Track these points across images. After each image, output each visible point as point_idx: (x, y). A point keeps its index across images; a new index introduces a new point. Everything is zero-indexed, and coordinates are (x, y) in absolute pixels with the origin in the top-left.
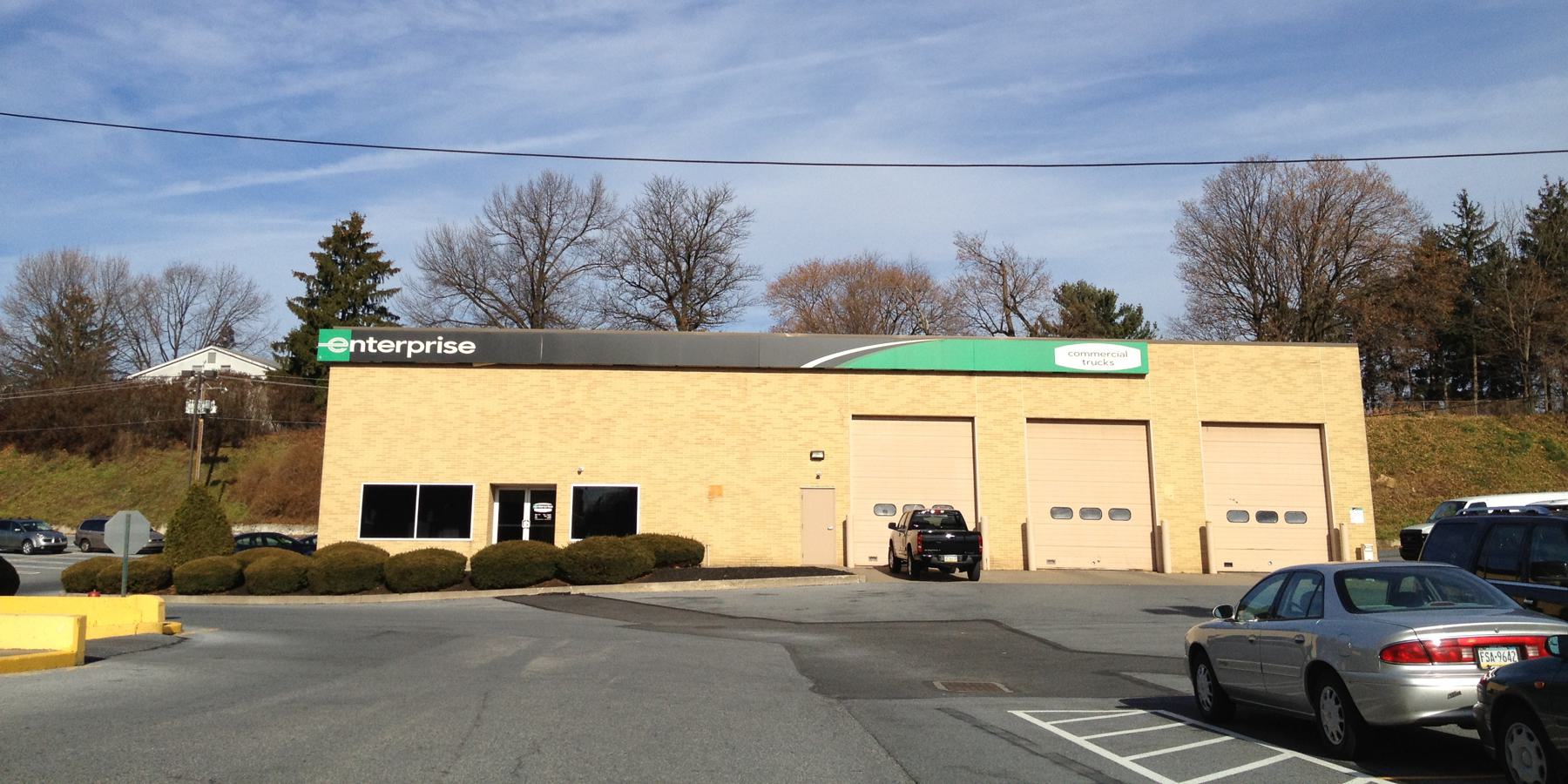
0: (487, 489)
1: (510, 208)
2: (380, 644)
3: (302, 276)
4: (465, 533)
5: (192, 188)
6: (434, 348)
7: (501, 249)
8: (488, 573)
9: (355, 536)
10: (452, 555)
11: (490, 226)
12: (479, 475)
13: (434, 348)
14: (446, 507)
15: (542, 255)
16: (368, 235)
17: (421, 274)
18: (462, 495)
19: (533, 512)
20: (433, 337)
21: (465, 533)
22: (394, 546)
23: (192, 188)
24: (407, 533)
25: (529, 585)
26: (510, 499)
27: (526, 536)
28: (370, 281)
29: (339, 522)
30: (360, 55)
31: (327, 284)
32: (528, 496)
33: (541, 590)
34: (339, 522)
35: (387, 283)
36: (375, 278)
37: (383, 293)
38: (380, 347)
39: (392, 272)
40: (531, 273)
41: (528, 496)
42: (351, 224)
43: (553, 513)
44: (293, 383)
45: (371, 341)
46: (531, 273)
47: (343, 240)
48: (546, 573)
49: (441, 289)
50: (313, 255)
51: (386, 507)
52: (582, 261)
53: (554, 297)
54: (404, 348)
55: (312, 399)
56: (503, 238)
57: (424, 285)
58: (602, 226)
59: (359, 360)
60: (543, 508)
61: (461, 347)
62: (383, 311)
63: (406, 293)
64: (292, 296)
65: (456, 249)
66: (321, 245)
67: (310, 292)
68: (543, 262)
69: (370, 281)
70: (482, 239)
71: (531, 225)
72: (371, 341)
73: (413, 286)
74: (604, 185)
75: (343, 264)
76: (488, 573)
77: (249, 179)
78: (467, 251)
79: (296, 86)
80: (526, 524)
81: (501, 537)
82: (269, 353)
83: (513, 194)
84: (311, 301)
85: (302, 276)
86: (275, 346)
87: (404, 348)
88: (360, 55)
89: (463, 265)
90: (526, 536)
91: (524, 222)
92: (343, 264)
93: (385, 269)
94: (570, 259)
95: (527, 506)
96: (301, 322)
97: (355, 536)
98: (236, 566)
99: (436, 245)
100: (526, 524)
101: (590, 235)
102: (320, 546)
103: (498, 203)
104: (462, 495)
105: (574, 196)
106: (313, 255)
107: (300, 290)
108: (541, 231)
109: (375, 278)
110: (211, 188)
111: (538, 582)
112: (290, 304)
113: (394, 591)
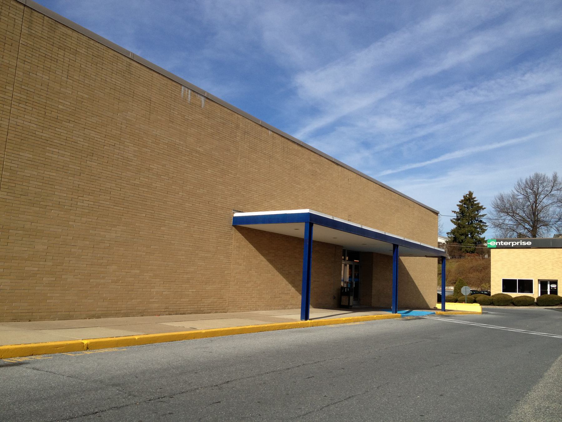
0: (537, 281)
1: (523, 187)
2: (526, 315)
3: (455, 212)
4: (531, 292)
5: (389, 172)
6: (519, 244)
7: (521, 201)
8: (540, 302)
9: (501, 292)
10: (530, 297)
11: (517, 193)
12: (535, 277)
13: (519, 244)
14: (526, 285)
15: (535, 202)
16: (475, 198)
17: (494, 209)
18: (530, 282)
19: (550, 287)
20: (519, 241)
21: (531, 292)
22: (513, 295)
23: (389, 172)
24: (515, 291)
25: (554, 306)
26: (543, 284)
27: (549, 293)
28: (476, 213)
29: (496, 288)
30: (443, 118)
31: (463, 214)
32: (549, 283)
33: (557, 307)
34: (496, 288)
35: (482, 213)
36: (478, 211)
37: (481, 216)
38: (504, 243)
39: (483, 209)
40: (532, 207)
41: (549, 283)
42: (469, 195)
43: (557, 287)
44: (455, 245)
45: (502, 242)
46: (532, 207)
47: (467, 200)
48: (558, 303)
49: (502, 214)
50: (458, 205)
51: (509, 285)
52: (550, 202)
53: (541, 215)
54: (511, 244)
55: (461, 250)
56: (521, 196)
57: (495, 213)
58: (558, 190)
59: (498, 247)
60: (554, 286)
61: (527, 243)
62: (481, 221)
63: (489, 215)
64: (452, 218)
65: (505, 201)
66: (460, 202)
67: (457, 217)
68: (536, 204)
69: (476, 213)
70: (514, 197)
71: (531, 191)
72: (502, 242)
73: (491, 213)
74: (558, 175)
75: (467, 208)
76: (540, 302)
77: (408, 167)
78: (509, 200)
79: (422, 133)
80: (549, 290)
81: (541, 294)
82: (446, 236)
83: (524, 181)
84: (458, 219)
85: (455, 212)
86: (448, 233)
87: (511, 244)
88: (443, 118)
89: (507, 205)
90: (549, 293)
91: (529, 191)
92: (467, 208)
93: (481, 208)
94: (546, 201)
95: (549, 285)
96: (455, 226)
97: (501, 292)
98: (473, 298)
99: (498, 200)
100: (549, 290)
101: (552, 193)
102: (492, 295)
103: (519, 185)
104: (530, 282)
105: (546, 180)
106: (458, 205)
107: (454, 216)
108: (534, 192)
109: (478, 211)
110: (394, 171)
111: (556, 305)
112: (451, 221)
113: (516, 306)
